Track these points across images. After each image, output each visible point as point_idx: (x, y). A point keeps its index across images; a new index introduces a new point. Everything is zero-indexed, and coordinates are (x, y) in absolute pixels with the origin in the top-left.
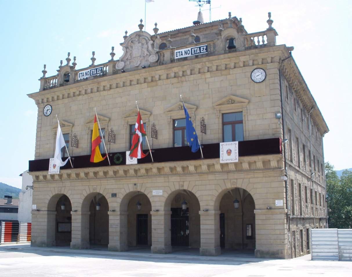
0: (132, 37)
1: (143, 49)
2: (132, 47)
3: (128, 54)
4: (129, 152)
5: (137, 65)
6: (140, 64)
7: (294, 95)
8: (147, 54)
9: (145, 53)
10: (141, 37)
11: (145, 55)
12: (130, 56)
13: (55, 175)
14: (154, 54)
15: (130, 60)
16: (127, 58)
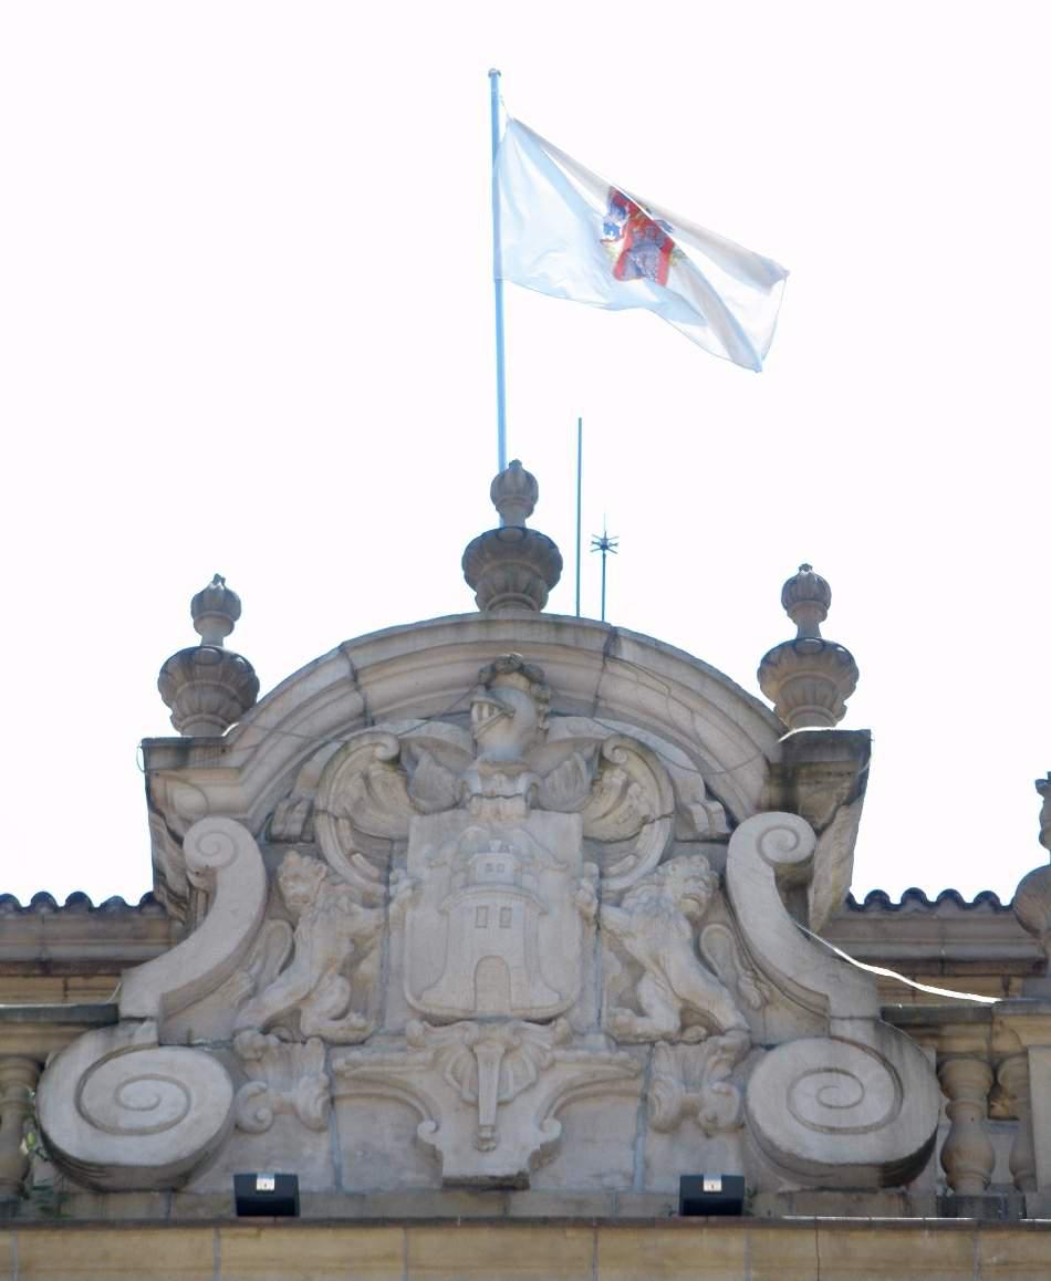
0: (379, 690)
1: (612, 916)
2: (386, 853)
3: (317, 945)
4: (772, 709)
5: (499, 1164)
6: (545, 1155)
7: (816, 760)
9: (648, 991)
10: (562, 728)
11: (662, 1018)
12: (335, 995)
13: (233, 1215)
14: (862, 1032)
15: (330, 1044)
16: (276, 1000)
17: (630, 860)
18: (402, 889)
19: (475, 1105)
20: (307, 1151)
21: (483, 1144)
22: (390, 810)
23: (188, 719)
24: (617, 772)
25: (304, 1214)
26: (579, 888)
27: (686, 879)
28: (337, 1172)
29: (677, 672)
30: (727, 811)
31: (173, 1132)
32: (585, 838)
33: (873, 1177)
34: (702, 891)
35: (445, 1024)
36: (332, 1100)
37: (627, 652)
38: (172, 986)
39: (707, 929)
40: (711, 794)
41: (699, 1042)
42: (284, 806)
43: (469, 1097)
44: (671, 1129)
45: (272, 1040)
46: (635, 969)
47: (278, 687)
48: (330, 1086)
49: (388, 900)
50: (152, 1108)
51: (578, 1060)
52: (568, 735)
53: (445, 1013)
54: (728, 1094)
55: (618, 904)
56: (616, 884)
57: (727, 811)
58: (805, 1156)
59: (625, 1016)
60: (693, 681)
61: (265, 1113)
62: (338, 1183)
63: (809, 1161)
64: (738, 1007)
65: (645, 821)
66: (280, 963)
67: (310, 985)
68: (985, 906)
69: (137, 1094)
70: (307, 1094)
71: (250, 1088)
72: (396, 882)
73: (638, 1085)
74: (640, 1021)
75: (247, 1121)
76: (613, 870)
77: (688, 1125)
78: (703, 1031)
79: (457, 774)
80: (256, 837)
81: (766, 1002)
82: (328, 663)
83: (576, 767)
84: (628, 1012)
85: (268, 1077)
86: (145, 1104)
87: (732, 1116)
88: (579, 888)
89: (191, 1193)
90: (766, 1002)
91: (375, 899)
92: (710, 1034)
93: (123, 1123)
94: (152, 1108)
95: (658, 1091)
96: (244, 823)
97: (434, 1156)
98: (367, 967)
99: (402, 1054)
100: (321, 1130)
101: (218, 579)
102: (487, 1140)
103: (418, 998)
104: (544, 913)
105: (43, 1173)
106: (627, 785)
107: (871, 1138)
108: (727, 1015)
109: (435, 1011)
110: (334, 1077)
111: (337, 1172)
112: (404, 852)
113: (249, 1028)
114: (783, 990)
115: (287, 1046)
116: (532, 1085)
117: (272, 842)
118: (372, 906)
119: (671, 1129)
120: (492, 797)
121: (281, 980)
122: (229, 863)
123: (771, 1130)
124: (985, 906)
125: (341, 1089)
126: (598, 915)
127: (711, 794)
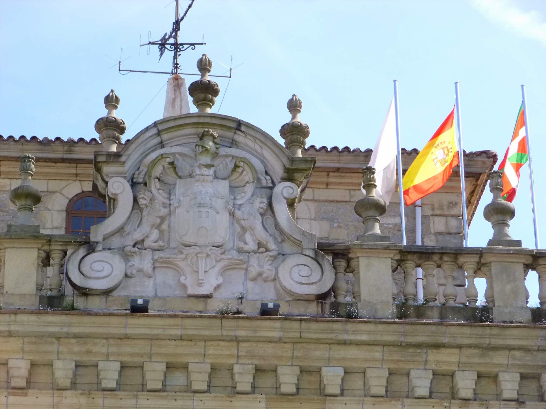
1: (238, 213)
5: (205, 290)
6: (218, 287)
8: (260, 245)
9: (248, 237)
11: (251, 246)
15: (154, 250)
16: (137, 236)
17: (243, 194)
18: (174, 203)
19: (197, 272)
20: (147, 284)
21: (200, 284)
22: (170, 177)
23: (105, 140)
24: (240, 168)
25: (150, 312)
26: (229, 204)
27: (260, 203)
28: (156, 290)
29: (258, 135)
30: (272, 179)
31: (107, 279)
32: (230, 186)
33: (313, 298)
34: (264, 206)
35: (188, 246)
36: (154, 268)
37: (243, 128)
38: (105, 233)
39: (265, 217)
40: (267, 173)
41: (263, 253)
42: (137, 172)
43: (196, 269)
44: (254, 279)
45: (136, 249)
46: (244, 230)
47: (136, 136)
48: (154, 264)
49: (170, 205)
50: (102, 270)
51: (228, 259)
52: (224, 154)
53: (189, 243)
54: (272, 270)
55: (239, 209)
56: (239, 202)
57: (272, 179)
58: (295, 292)
59: (241, 245)
60: (263, 139)
61: (134, 272)
62: (156, 294)
63: (296, 293)
64: (275, 244)
65: (247, 182)
66: (137, 224)
67: (146, 230)
68: (323, 151)
69: (97, 266)
70: (147, 266)
71: (130, 264)
72: (172, 200)
73: (244, 266)
74: (246, 246)
75: (129, 273)
76: (238, 197)
77: (259, 279)
78: (264, 250)
79: (192, 166)
80: (128, 182)
81: (283, 241)
82: (151, 128)
83: (227, 164)
84: (242, 243)
85: (136, 261)
86: (99, 270)
87: (273, 277)
88: (229, 204)
89: (113, 296)
90: (283, 241)
91: (166, 205)
92: (266, 251)
93: (92, 276)
94: (102, 270)
95: (251, 269)
96: (125, 178)
97: (185, 287)
98: (164, 227)
99: (175, 256)
100: (150, 277)
101: (112, 91)
102: (201, 283)
103: (181, 239)
104: (218, 213)
105: (69, 290)
106: (243, 171)
107: (314, 286)
108: (272, 246)
109: (185, 243)
110: (155, 261)
111: (156, 290)
112: (174, 188)
113: (129, 246)
114: (288, 238)
115: (140, 251)
116: (214, 267)
117: (134, 184)
118: (165, 207)
119: (254, 279)
120: (202, 175)
121: (139, 230)
122: (121, 193)
123: (286, 284)
124: (323, 151)
125: (157, 265)
126: (234, 213)
127: (267, 173)
